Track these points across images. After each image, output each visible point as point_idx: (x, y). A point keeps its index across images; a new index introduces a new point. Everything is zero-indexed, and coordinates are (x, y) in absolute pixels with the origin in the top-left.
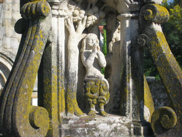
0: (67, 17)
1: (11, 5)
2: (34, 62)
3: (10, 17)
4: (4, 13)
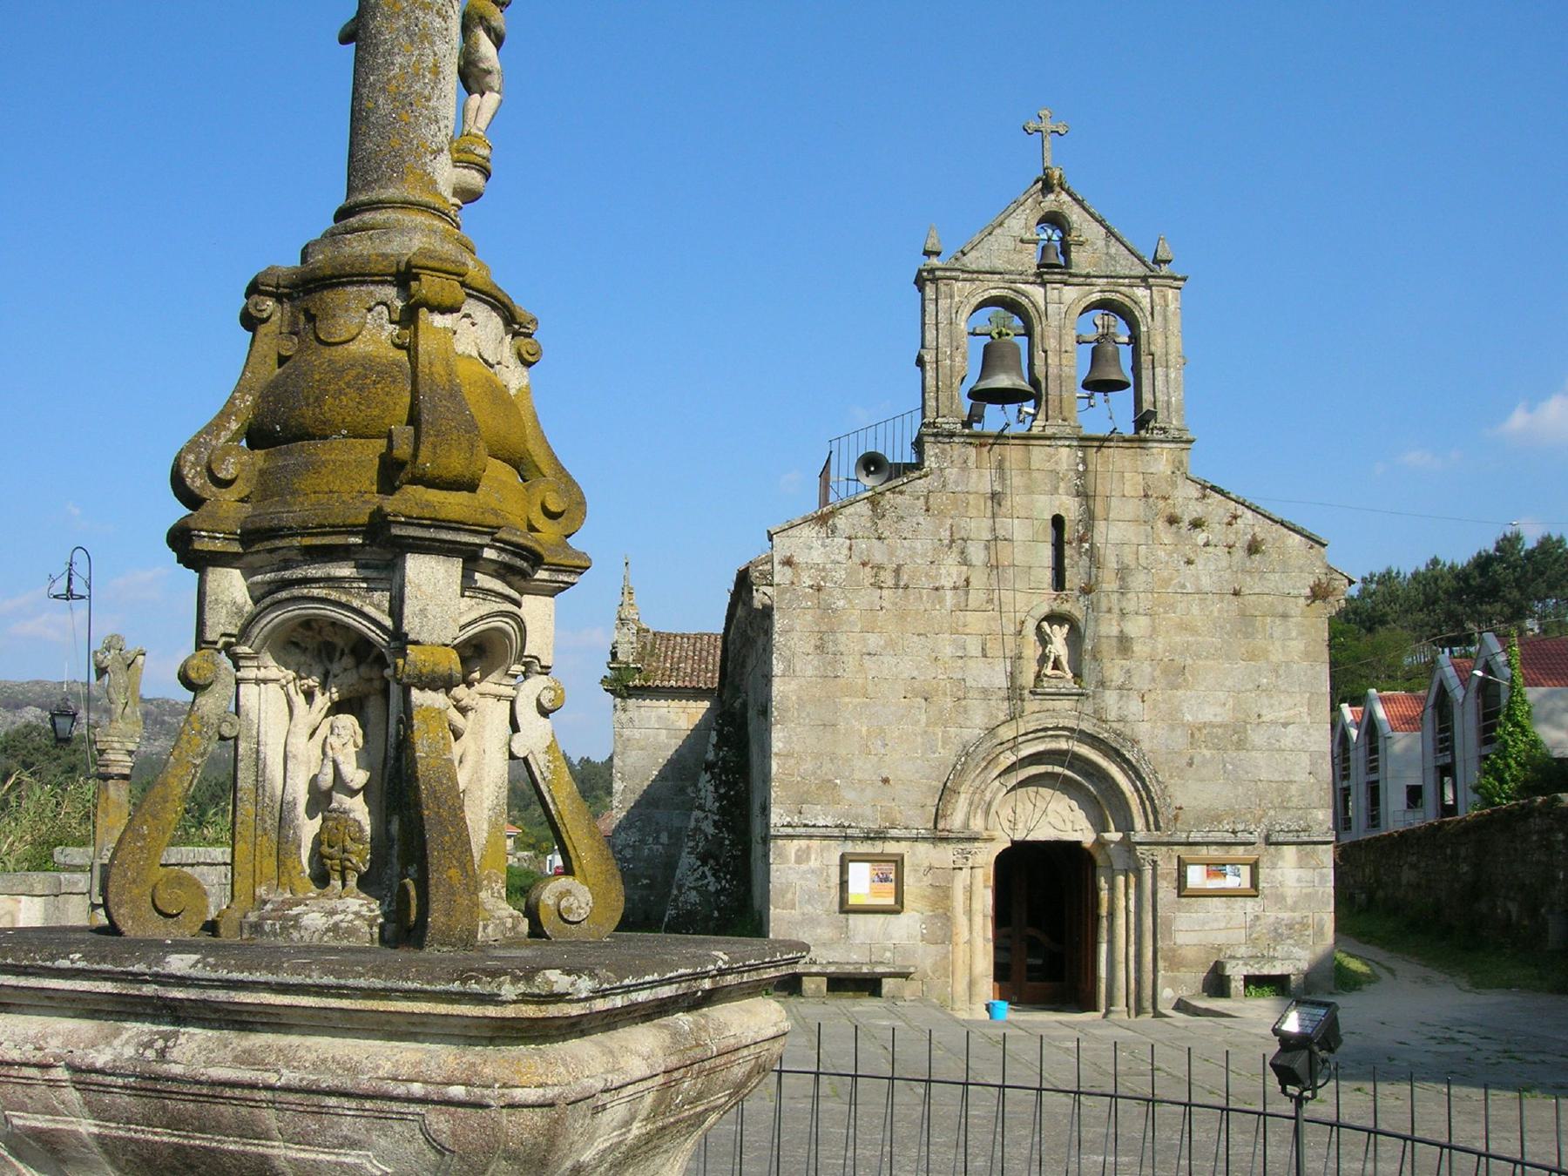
0: (284, 682)
1: (1115, 597)
2: (171, 780)
3: (1115, 631)
4: (1096, 620)
